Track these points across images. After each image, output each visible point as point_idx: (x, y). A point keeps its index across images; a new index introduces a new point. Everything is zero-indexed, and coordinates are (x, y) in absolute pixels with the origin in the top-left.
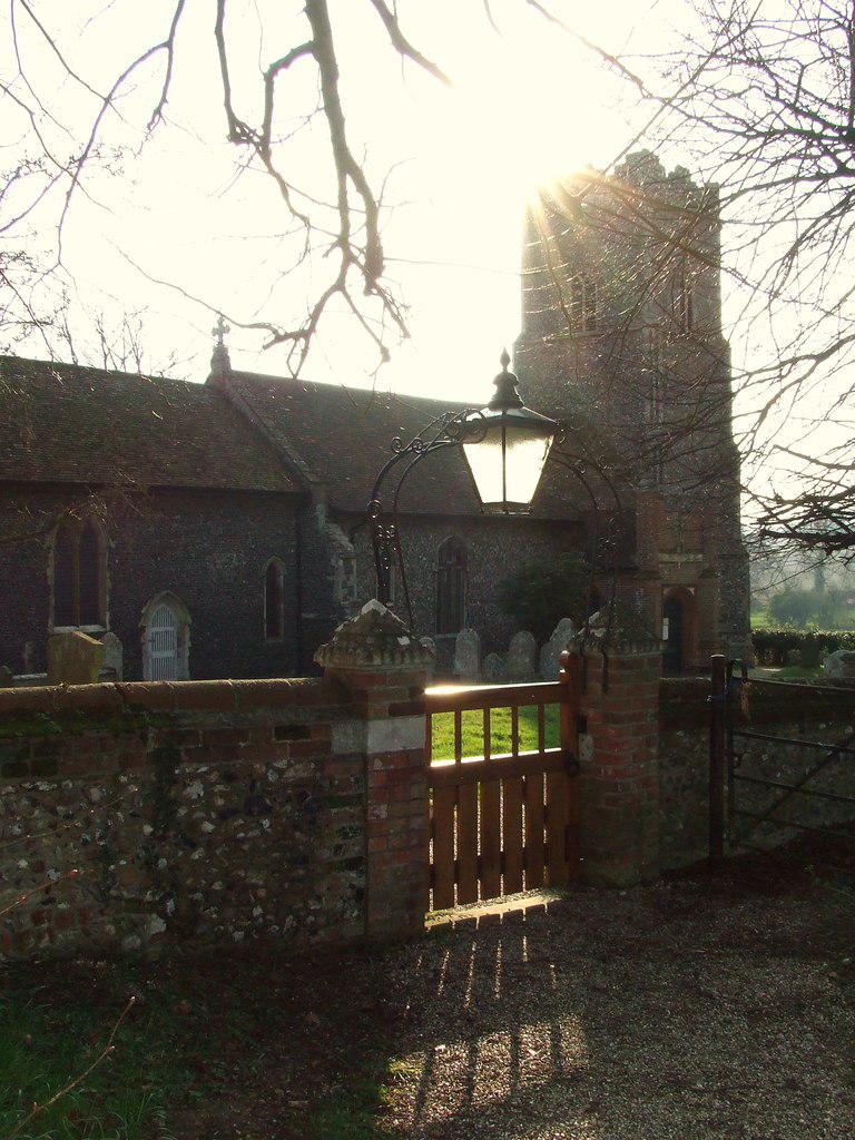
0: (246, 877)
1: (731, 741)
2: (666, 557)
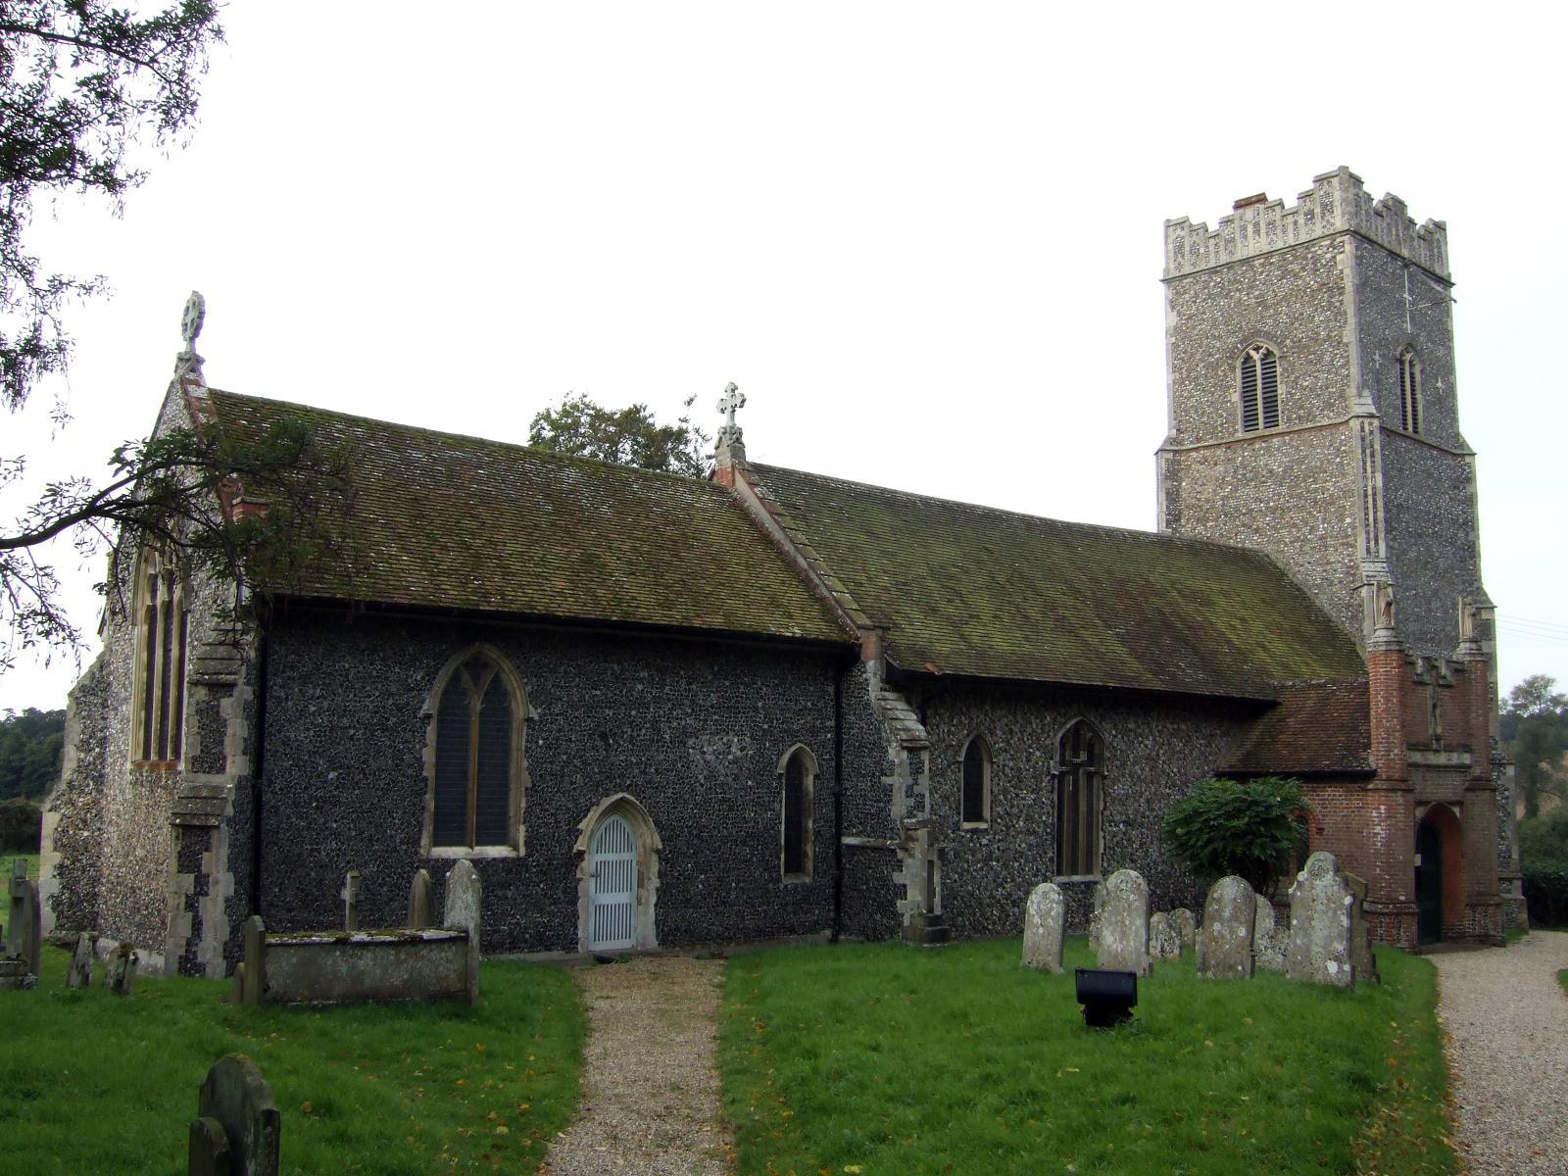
2: (1417, 757)
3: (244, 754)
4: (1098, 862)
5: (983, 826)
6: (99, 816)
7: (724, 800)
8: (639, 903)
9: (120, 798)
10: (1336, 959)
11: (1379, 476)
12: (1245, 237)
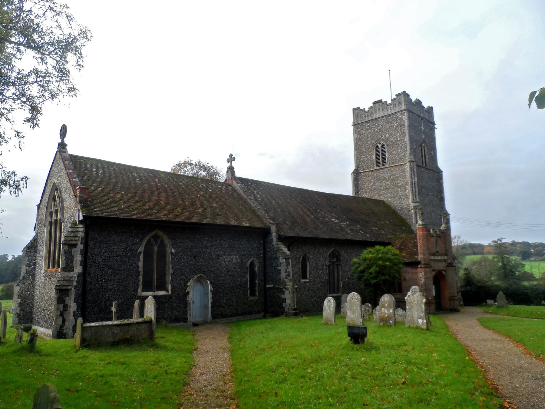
2: (432, 257)
3: (80, 265)
4: (341, 290)
5: (307, 280)
6: (33, 287)
7: (231, 275)
9: (40, 281)
10: (422, 319)
11: (416, 178)
12: (376, 112)
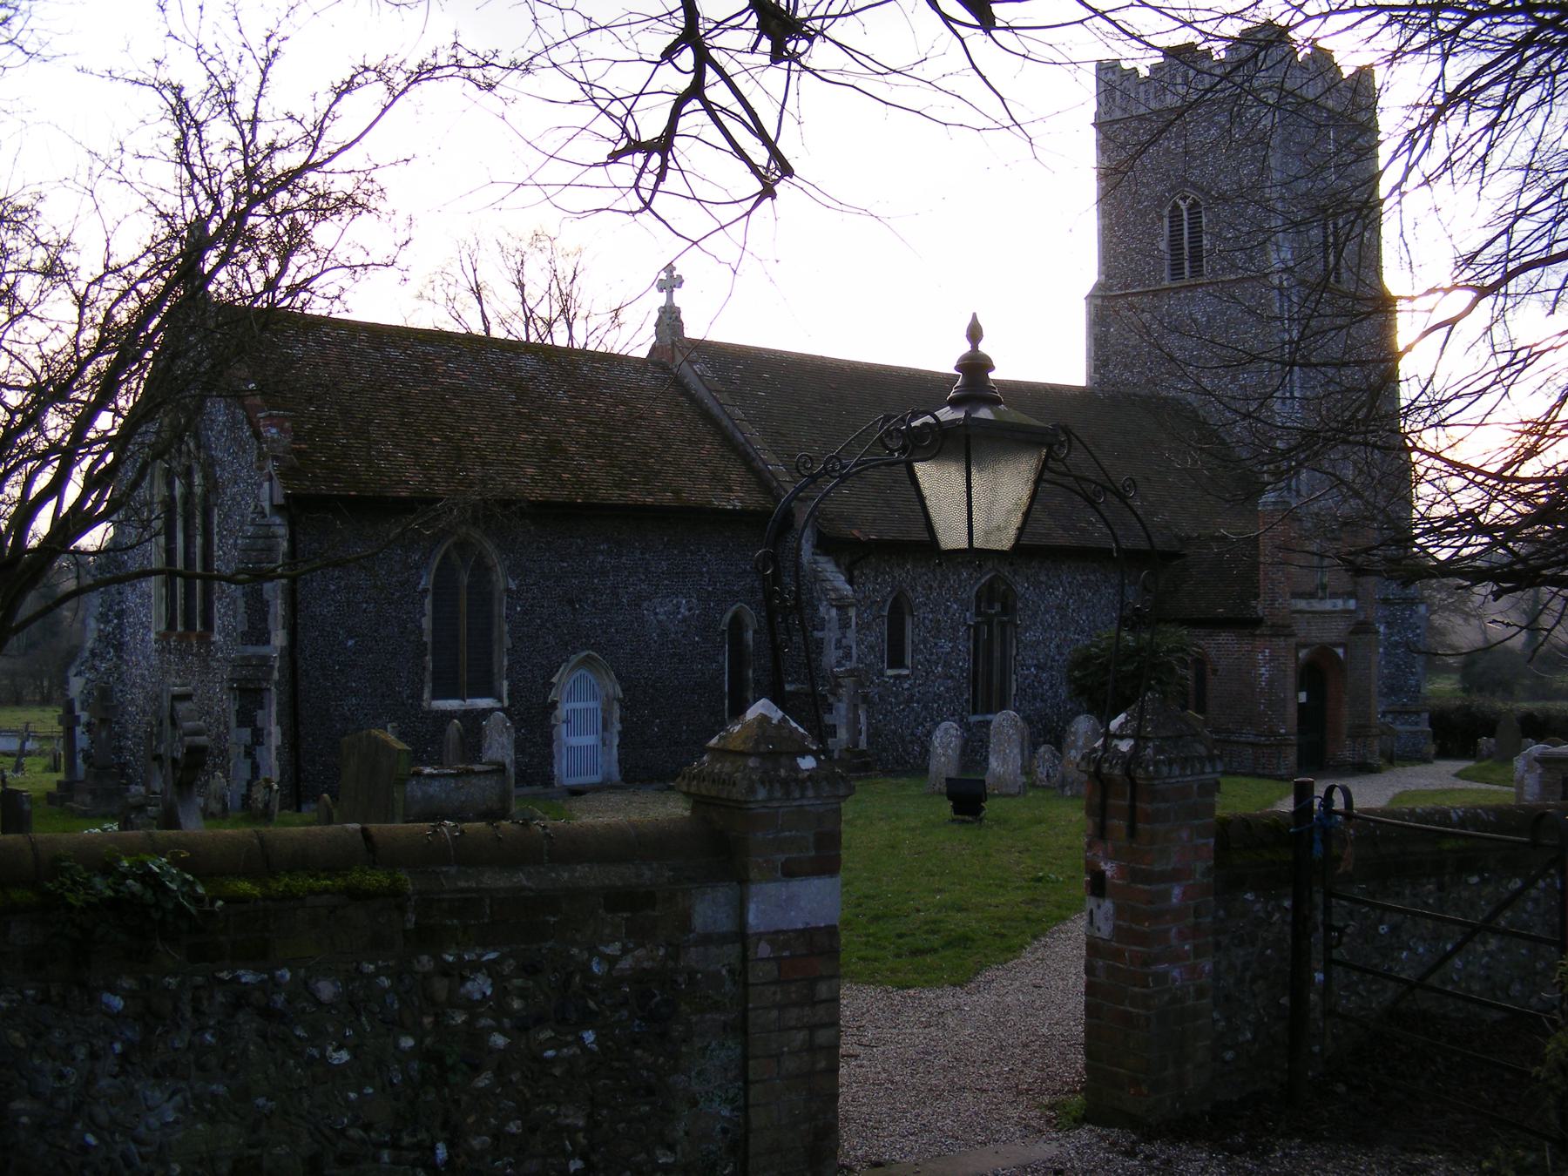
0: (557, 1115)
1: (1327, 909)
2: (1302, 604)
5: (905, 672)
8: (604, 744)
